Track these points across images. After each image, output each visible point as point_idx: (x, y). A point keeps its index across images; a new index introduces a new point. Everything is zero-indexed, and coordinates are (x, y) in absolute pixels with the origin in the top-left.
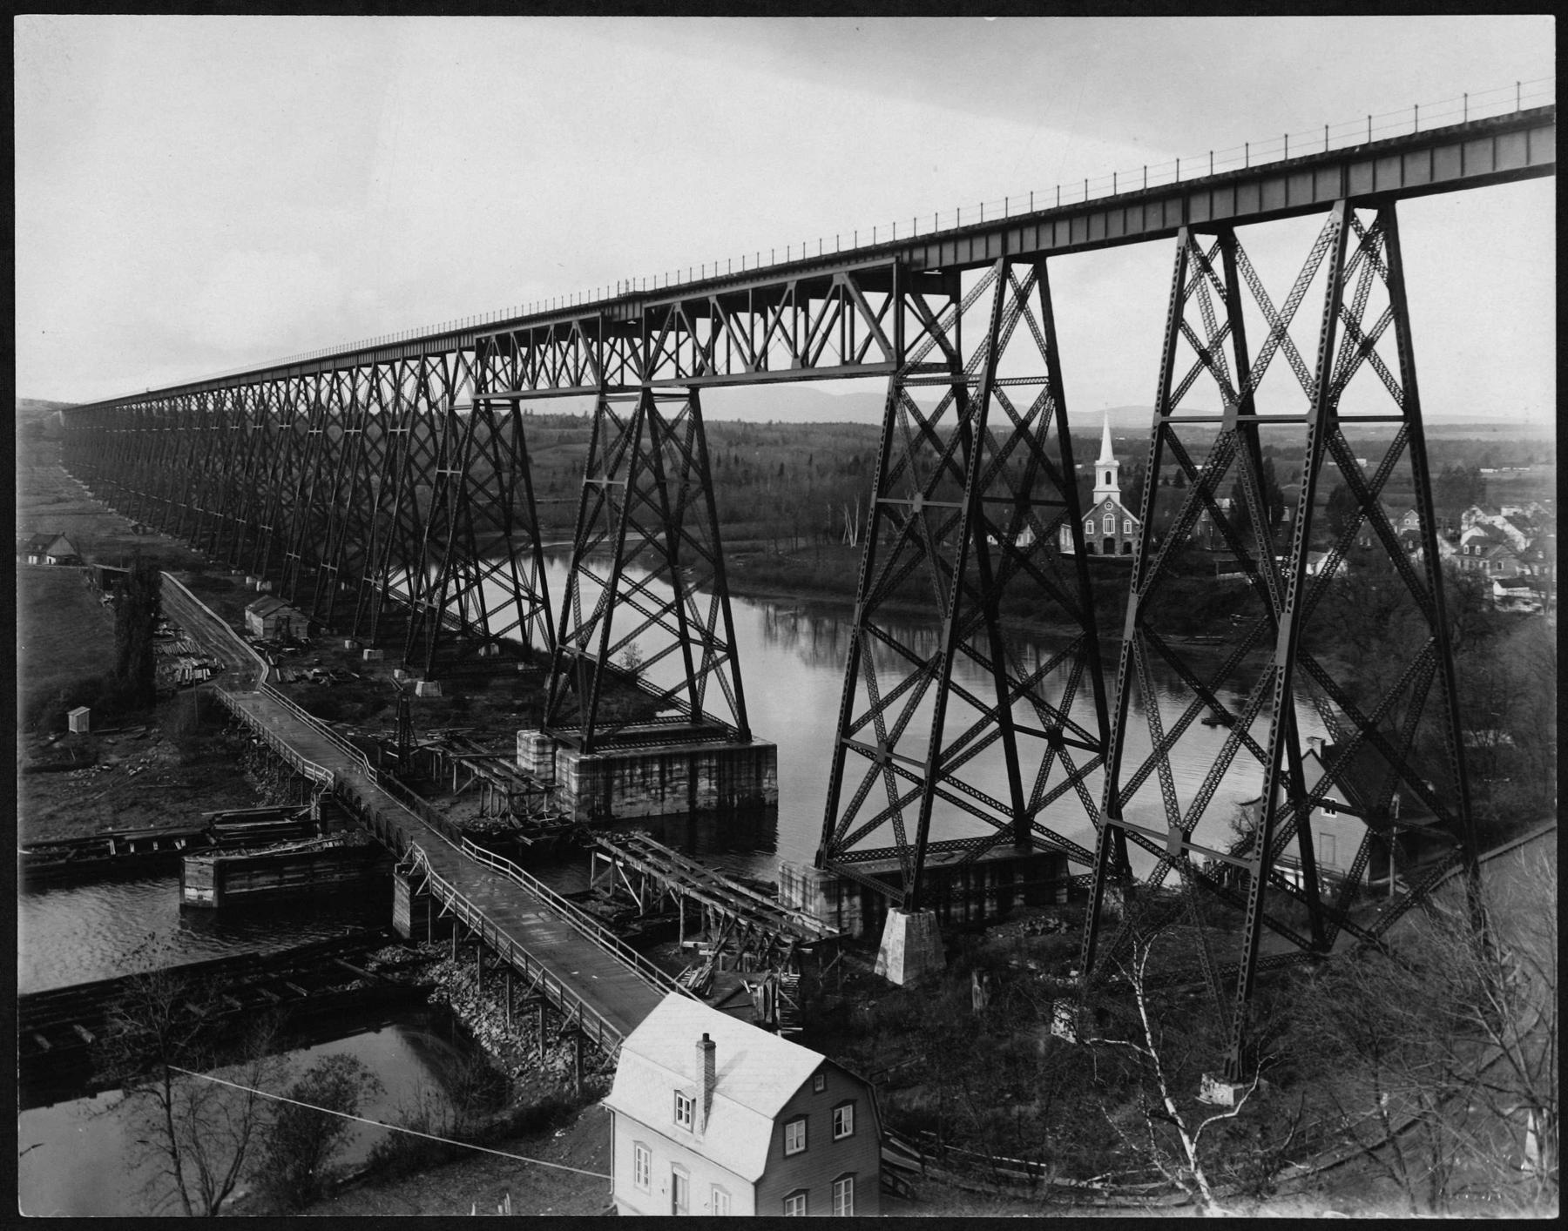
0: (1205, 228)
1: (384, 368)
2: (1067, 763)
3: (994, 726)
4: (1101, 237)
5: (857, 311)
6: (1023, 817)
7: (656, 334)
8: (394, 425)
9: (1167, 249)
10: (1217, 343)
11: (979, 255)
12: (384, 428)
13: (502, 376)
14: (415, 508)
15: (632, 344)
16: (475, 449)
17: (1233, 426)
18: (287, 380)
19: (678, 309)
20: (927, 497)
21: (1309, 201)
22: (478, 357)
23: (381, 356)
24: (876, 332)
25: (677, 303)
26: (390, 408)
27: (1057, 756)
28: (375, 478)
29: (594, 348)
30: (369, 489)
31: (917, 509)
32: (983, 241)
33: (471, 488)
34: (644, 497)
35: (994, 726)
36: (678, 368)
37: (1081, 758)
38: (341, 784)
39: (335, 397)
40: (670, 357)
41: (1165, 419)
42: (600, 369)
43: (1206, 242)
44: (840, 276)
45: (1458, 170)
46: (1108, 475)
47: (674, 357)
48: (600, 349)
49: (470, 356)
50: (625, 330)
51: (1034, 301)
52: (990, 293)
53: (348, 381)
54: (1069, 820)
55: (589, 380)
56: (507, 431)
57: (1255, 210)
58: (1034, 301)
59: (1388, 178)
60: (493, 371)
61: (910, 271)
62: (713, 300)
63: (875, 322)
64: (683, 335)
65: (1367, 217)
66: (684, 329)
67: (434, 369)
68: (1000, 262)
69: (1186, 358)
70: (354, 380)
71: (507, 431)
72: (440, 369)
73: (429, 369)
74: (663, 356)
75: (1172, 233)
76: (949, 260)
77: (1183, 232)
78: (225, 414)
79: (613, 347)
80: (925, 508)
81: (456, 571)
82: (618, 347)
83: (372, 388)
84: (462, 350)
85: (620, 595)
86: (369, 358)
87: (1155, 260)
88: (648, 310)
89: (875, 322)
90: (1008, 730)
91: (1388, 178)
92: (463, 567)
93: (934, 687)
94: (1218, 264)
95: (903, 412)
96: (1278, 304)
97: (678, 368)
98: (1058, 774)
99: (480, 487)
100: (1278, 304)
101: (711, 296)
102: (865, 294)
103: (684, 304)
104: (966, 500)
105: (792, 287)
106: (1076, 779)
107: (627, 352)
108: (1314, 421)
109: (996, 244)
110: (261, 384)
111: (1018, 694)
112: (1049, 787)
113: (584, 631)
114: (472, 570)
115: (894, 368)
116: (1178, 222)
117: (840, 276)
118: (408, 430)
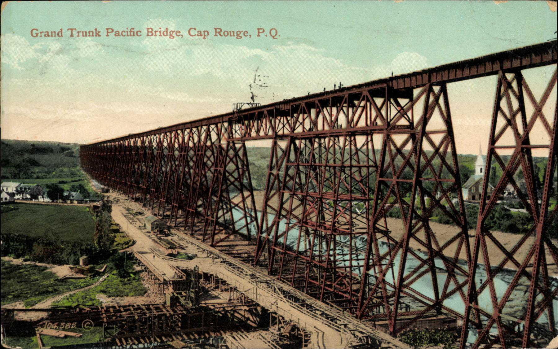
0: (510, 71)
1: (194, 129)
2: (456, 282)
3: (426, 267)
4: (461, 76)
5: (372, 107)
6: (438, 305)
7: (295, 115)
8: (198, 151)
9: (493, 80)
10: (514, 116)
11: (419, 83)
12: (195, 152)
13: (238, 132)
14: (207, 183)
15: (287, 119)
16: (228, 159)
17: (520, 149)
18: (171, 133)
19: (303, 105)
20: (398, 178)
21: (483, 72)
22: (229, 125)
23: (193, 125)
24: (379, 114)
25: (303, 103)
26: (197, 145)
27: (452, 279)
28: (192, 171)
29: (273, 121)
30: (190, 175)
31: (394, 182)
32: (446, 72)
33: (227, 174)
34: (292, 178)
35: (426, 267)
36: (304, 128)
37: (461, 279)
38: (132, 253)
39: (176, 140)
40: (301, 124)
41: (493, 147)
42: (274, 129)
43: (509, 76)
44: (365, 92)
45: (447, 77)
46: (481, 169)
47: (302, 124)
48: (275, 122)
49: (226, 124)
50: (284, 114)
51: (441, 101)
52: (423, 98)
53: (181, 134)
54: (456, 304)
55: (270, 133)
56: (241, 153)
57: (476, 73)
58: (441, 101)
59: (516, 63)
60: (235, 130)
61: (392, 89)
62: (317, 102)
63: (379, 110)
64: (306, 115)
65: (436, 89)
66: (306, 113)
67: (213, 129)
68: (428, 85)
69: (501, 122)
70: (183, 133)
71: (241, 153)
72: (215, 129)
73: (211, 129)
74: (298, 124)
75: (495, 73)
76: (407, 85)
77: (500, 73)
78: (145, 147)
79: (280, 121)
80: (397, 182)
81: (222, 206)
82: (282, 121)
83: (190, 137)
84: (223, 122)
85: (283, 216)
86: (189, 126)
87: (490, 82)
88: (292, 106)
89: (379, 110)
90: (433, 270)
91: (516, 63)
92: (225, 204)
93: (400, 252)
94: (514, 85)
95: (390, 145)
96: (538, 99)
97: (304, 128)
98: (452, 286)
99: (231, 174)
100: (538, 99)
101: (316, 100)
102: (374, 99)
103: (306, 104)
104: (414, 179)
105: (347, 96)
106: (459, 288)
107: (285, 122)
108: (552, 148)
109: (426, 77)
110: (160, 134)
111: (436, 256)
112: (449, 291)
113: (269, 230)
114: (228, 206)
115: (386, 127)
116: (427, 82)
117: (365, 92)
118: (203, 153)
